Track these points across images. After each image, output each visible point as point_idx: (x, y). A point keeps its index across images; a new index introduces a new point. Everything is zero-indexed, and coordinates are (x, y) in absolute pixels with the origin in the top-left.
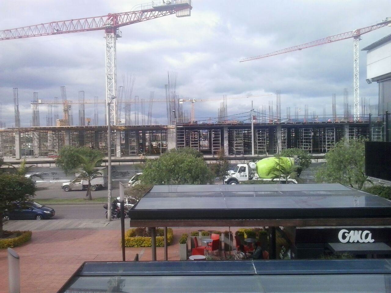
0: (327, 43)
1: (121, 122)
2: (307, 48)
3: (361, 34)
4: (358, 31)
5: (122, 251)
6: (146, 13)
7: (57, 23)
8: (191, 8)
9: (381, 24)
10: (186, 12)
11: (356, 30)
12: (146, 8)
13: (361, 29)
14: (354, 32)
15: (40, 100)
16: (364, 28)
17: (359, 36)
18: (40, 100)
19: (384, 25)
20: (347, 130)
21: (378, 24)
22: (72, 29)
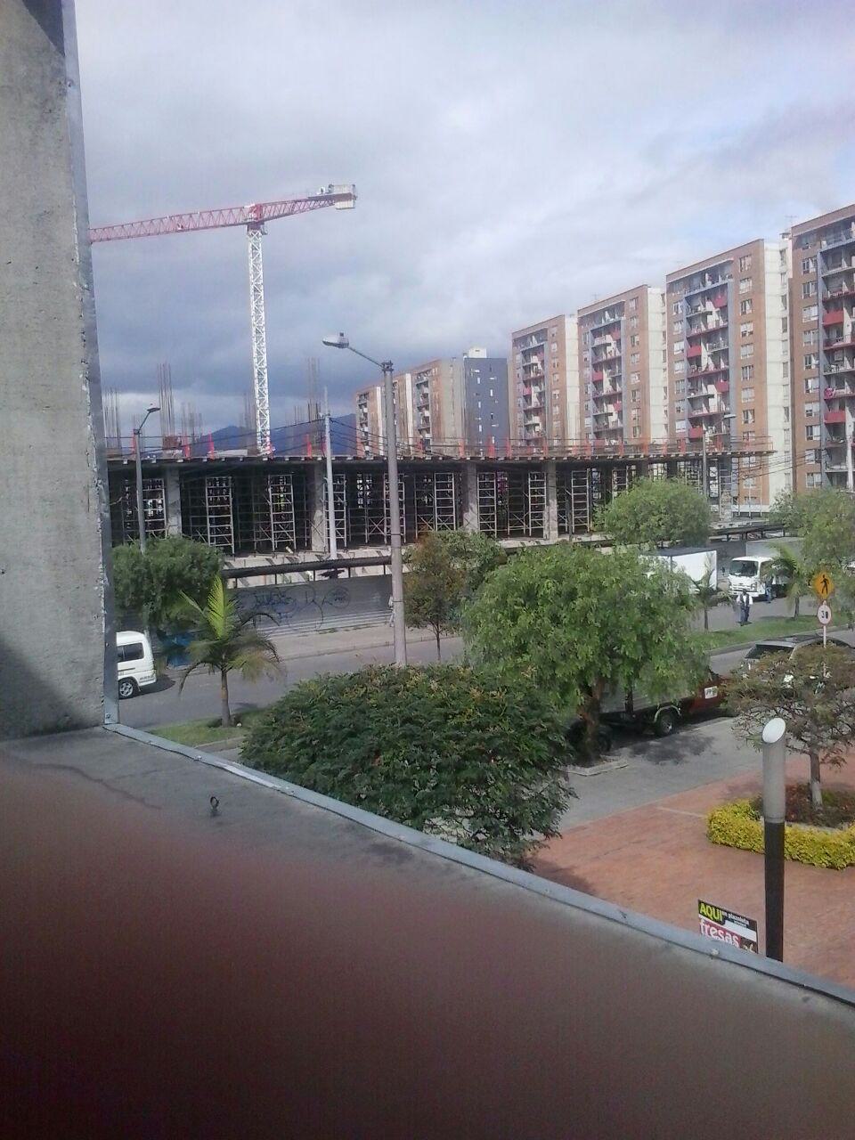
0: (153, 234)
1: (259, 453)
2: (108, 239)
3: (267, 220)
4: (258, 208)
5: (763, 875)
6: (299, 204)
7: (180, 216)
8: (355, 198)
9: (317, 199)
10: (349, 204)
11: (254, 205)
12: (299, 198)
13: (265, 205)
14: (248, 211)
15: (675, 345)
16: (275, 204)
17: (262, 222)
18: (675, 345)
19: (323, 202)
20: (474, 484)
21: (311, 199)
22: (201, 226)
